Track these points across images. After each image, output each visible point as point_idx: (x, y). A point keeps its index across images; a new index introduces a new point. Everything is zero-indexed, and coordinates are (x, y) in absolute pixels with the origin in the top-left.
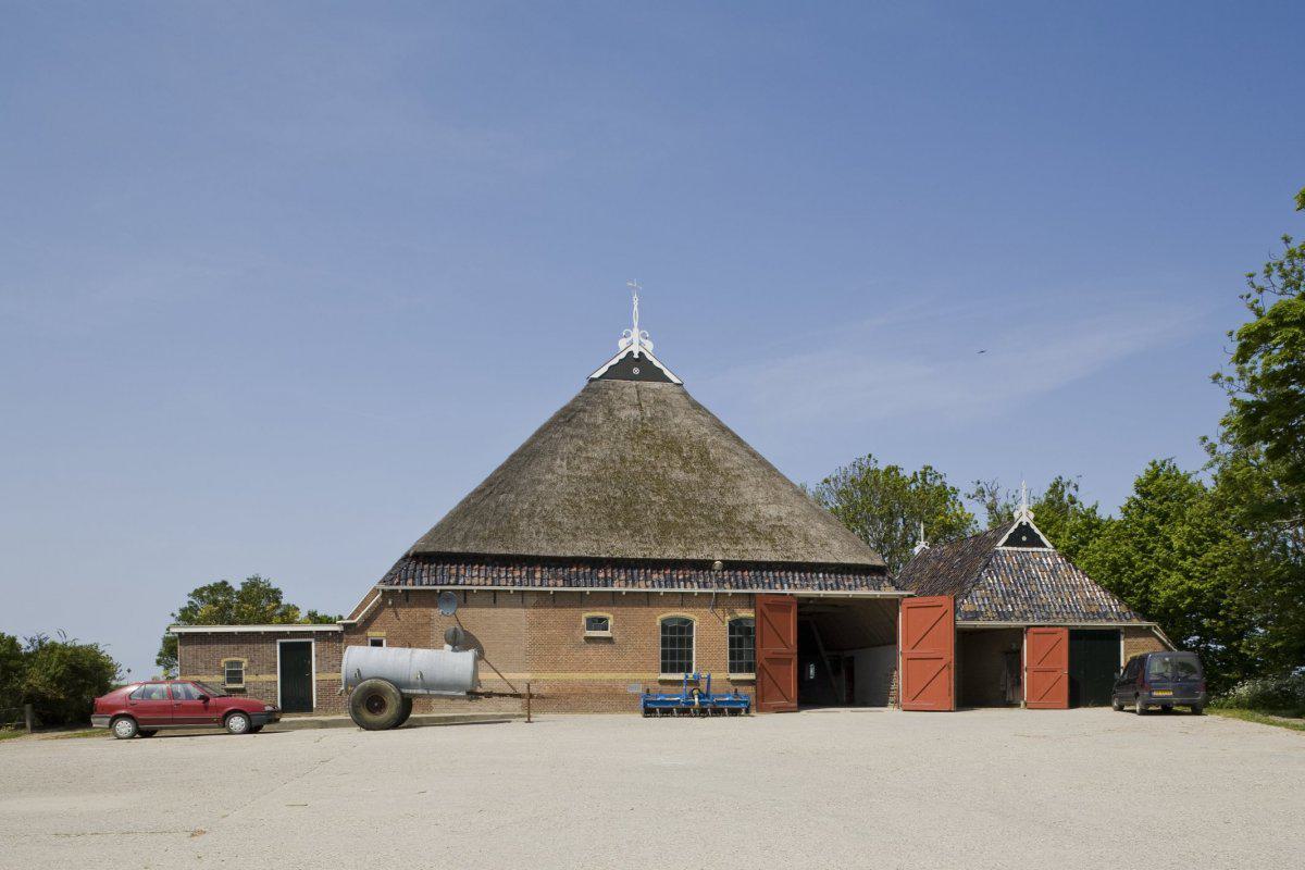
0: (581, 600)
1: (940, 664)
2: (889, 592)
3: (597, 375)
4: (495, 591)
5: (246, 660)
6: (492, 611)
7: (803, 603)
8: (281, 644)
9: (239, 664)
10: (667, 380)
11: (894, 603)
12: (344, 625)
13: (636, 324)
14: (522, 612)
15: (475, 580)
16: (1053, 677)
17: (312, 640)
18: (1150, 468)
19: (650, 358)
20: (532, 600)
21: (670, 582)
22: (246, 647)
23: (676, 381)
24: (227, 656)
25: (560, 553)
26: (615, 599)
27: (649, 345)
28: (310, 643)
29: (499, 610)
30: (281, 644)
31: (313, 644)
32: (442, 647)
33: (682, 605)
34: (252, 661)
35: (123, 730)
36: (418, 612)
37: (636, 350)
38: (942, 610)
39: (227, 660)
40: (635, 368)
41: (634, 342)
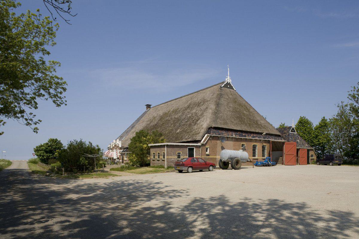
0: (241, 140)
1: (293, 156)
2: (283, 141)
3: (222, 86)
4: (228, 137)
5: (181, 152)
6: (227, 142)
7: (273, 142)
8: (188, 148)
9: (180, 153)
10: (233, 89)
11: (283, 143)
12: (202, 144)
13: (229, 74)
14: (232, 142)
15: (225, 134)
16: (304, 158)
17: (194, 148)
18: (323, 118)
19: (231, 84)
20: (233, 139)
21: (253, 137)
22: (182, 149)
23: (235, 90)
24: (178, 151)
25: (251, 131)
26: (246, 140)
27: (231, 81)
28: (193, 149)
29: (228, 142)
30: (188, 148)
31: (195, 149)
32: (128, 146)
33: (256, 142)
34: (183, 153)
35: (191, 170)
36: (215, 141)
37: (229, 81)
38: (294, 145)
39: (178, 152)
40: (228, 86)
41: (228, 80)
